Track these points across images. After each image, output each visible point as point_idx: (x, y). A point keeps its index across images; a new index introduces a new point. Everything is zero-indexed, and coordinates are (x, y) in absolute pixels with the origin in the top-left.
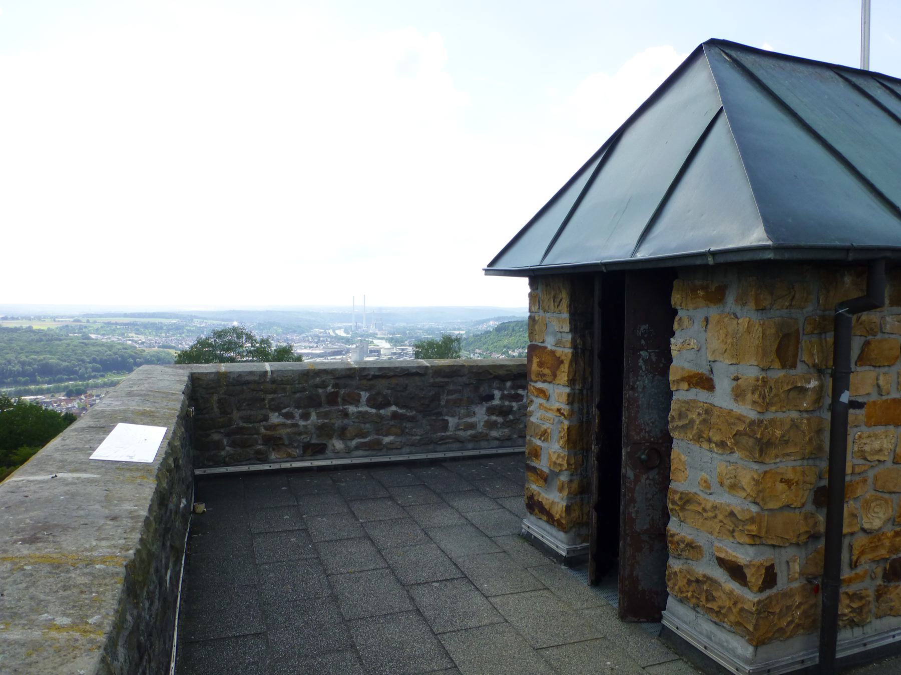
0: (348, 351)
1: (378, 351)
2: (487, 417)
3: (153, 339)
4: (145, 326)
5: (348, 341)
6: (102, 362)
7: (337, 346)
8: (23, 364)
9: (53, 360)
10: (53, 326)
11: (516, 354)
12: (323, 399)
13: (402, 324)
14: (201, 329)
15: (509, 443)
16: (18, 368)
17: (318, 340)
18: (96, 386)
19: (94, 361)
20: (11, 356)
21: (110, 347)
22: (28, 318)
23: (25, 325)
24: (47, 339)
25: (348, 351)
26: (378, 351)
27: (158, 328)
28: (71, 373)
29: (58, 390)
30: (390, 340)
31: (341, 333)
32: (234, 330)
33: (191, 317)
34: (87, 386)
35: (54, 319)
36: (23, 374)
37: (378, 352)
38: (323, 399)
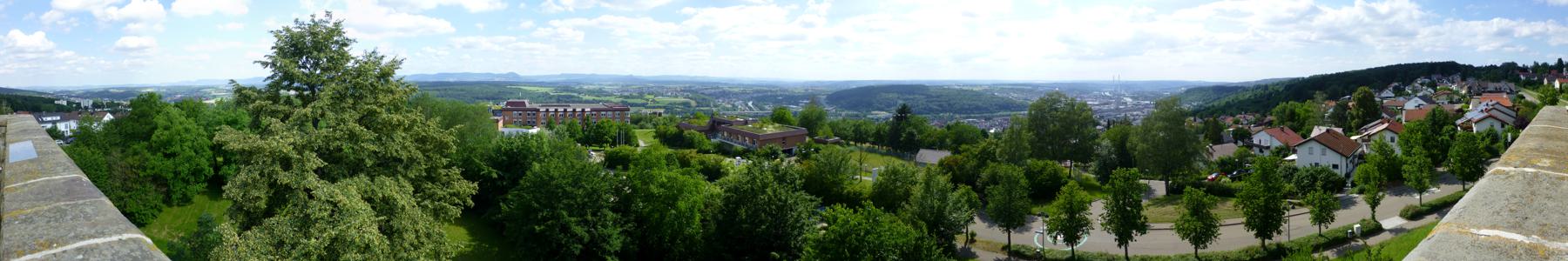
0: (1111, 103)
1: (1126, 103)
2: (1333, 104)
3: (1020, 96)
4: (1018, 90)
5: (1111, 98)
6: (1000, 106)
7: (1105, 101)
8: (969, 105)
9: (980, 104)
10: (980, 89)
11: (1195, 104)
12: (1093, 165)
13: (1138, 90)
14: (1041, 92)
15: (1559, 123)
16: (967, 107)
17: (1096, 98)
18: (997, 116)
19: (996, 105)
20: (965, 102)
21: (1003, 99)
22: (971, 86)
23: (971, 88)
24: (978, 95)
25: (1111, 103)
26: (1126, 103)
27: (1022, 91)
28: (987, 110)
29: (981, 117)
30: (1131, 98)
31: (1107, 94)
32: (1057, 93)
33: (1037, 86)
34: (993, 117)
35: (981, 86)
36: (969, 109)
37: (1125, 103)
38: (1093, 165)
